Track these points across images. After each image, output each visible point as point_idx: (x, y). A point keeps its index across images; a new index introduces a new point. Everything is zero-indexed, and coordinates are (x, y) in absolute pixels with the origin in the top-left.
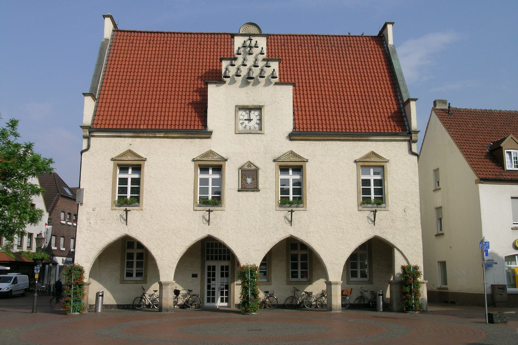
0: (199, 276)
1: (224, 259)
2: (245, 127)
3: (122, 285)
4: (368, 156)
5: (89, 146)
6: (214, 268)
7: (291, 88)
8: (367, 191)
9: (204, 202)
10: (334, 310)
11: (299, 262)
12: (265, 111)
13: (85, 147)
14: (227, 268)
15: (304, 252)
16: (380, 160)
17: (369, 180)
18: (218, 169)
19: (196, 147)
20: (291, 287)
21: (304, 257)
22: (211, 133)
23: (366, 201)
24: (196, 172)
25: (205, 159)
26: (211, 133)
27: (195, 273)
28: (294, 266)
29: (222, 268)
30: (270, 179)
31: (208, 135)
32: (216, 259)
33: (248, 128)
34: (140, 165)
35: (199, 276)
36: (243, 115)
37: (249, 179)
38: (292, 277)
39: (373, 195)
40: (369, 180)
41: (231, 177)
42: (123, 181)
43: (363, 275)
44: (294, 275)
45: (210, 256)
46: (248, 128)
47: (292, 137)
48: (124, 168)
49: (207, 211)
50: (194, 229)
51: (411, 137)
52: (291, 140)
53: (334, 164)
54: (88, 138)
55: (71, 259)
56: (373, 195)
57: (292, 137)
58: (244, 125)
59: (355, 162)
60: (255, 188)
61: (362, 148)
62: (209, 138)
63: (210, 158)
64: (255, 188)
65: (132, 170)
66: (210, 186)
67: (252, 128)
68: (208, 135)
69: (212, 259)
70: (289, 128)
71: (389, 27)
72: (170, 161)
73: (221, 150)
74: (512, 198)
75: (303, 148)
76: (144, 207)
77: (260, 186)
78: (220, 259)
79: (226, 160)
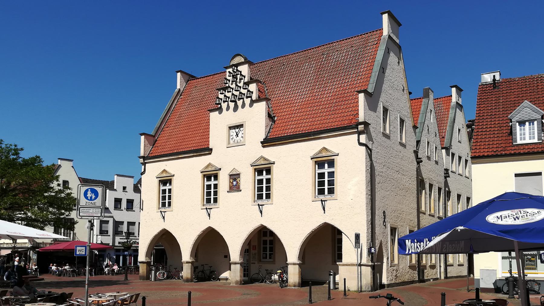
4: (320, 152)
5: (145, 169)
8: (321, 184)
13: (143, 171)
15: (272, 238)
16: (329, 154)
19: (200, 163)
22: (211, 149)
26: (211, 149)
28: (265, 249)
30: (248, 181)
31: (208, 151)
33: (236, 141)
36: (233, 132)
39: (325, 186)
41: (224, 182)
42: (321, 175)
46: (236, 141)
48: (209, 178)
52: (264, 147)
53: (294, 162)
54: (144, 164)
56: (325, 186)
57: (267, 142)
61: (312, 147)
62: (210, 154)
67: (239, 141)
68: (208, 151)
70: (262, 137)
72: (187, 172)
74: (517, 175)
75: (272, 153)
79: (220, 169)
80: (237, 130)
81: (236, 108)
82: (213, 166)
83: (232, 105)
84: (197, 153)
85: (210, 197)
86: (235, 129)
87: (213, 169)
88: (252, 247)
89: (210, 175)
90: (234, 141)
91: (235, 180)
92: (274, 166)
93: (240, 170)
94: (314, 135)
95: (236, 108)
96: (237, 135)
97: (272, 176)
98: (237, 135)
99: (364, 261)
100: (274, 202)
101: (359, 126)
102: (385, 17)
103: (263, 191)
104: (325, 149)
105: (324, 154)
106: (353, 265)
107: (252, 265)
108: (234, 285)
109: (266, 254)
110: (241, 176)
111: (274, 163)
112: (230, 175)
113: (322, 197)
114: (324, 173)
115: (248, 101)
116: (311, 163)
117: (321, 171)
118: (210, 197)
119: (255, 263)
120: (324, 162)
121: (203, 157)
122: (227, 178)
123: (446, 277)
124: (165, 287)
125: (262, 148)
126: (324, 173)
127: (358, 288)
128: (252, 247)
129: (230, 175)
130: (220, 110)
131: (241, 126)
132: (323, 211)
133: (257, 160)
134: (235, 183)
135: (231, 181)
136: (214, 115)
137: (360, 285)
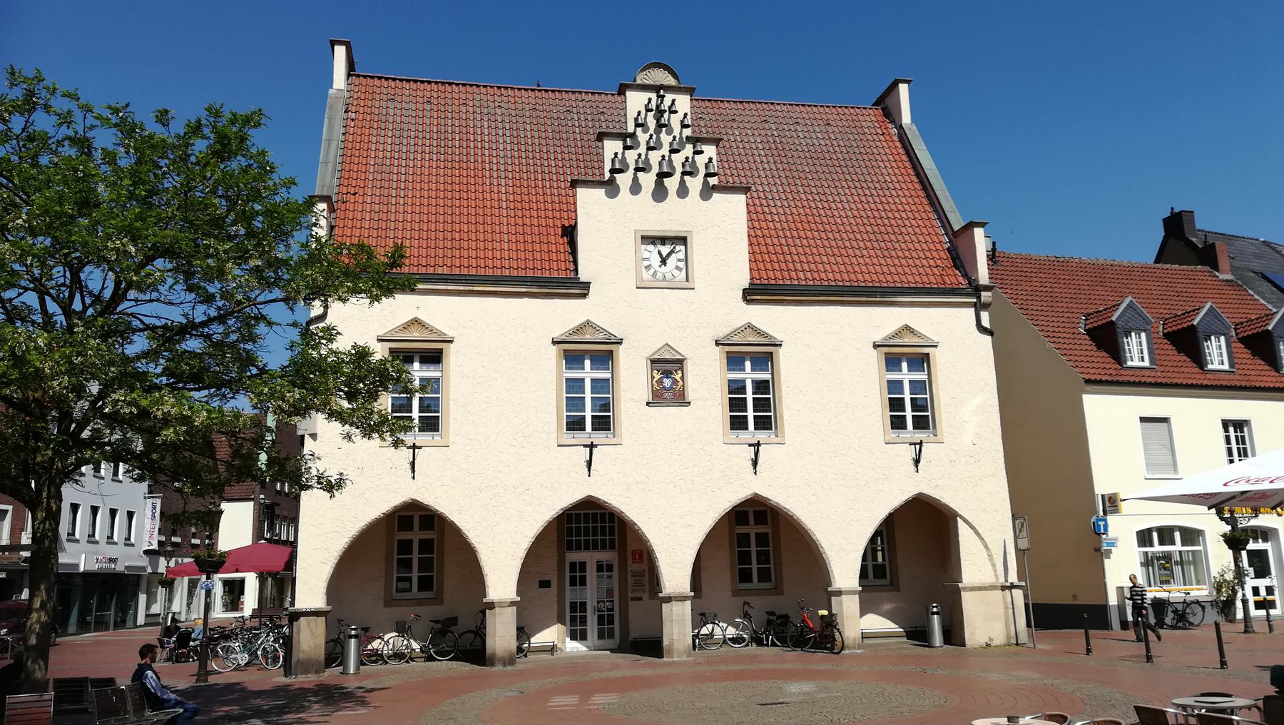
0: (554, 584)
1: (604, 548)
2: (655, 274)
3: (388, 610)
4: (897, 334)
6: (583, 566)
7: (740, 199)
8: (761, 405)
9: (575, 425)
10: (849, 648)
11: (415, 556)
12: (694, 242)
14: (610, 568)
16: (916, 341)
17: (901, 382)
18: (604, 358)
19: (561, 315)
20: (740, 600)
21: (426, 546)
22: (586, 285)
23: (575, 425)
24: (558, 365)
25: (897, 341)
26: (586, 285)
27: (547, 578)
28: (405, 565)
29: (600, 568)
30: (707, 380)
31: (581, 289)
32: (587, 548)
33: (659, 276)
34: (440, 351)
35: (554, 584)
36: (652, 253)
37: (668, 380)
38: (741, 581)
39: (911, 412)
40: (901, 382)
41: (632, 378)
42: (895, 386)
43: (764, 575)
44: (745, 576)
45: (590, 543)
46: (659, 276)
47: (752, 294)
49: (585, 446)
50: (560, 482)
51: (979, 297)
53: (827, 351)
55: (1155, 535)
56: (911, 412)
57: (752, 294)
58: (652, 271)
59: (876, 346)
60: (680, 399)
61: (884, 320)
62: (584, 296)
63: (588, 337)
64: (680, 399)
65: (752, 365)
66: (588, 395)
67: (668, 276)
68: (581, 289)
69: (578, 548)
71: (903, 89)
73: (610, 323)
74: (1143, 420)
75: (774, 319)
76: (452, 439)
77: (690, 395)
78: (595, 548)
79: (620, 342)
80: (665, 250)
81: (660, 193)
82: (597, 329)
83: (648, 180)
84: (867, 296)
85: (591, 417)
86: (653, 243)
87: (599, 337)
88: (629, 556)
89: (588, 352)
90: (655, 274)
91: (667, 374)
92: (621, 348)
93: (683, 350)
94: (883, 294)
95: (660, 193)
96: (664, 262)
97: (559, 374)
98: (664, 262)
99: (1013, 578)
100: (786, 440)
101: (983, 294)
102: (340, 51)
103: (753, 409)
104: (907, 328)
105: (908, 340)
106: (992, 588)
107: (630, 603)
108: (684, 658)
109: (410, 580)
110: (689, 367)
111: (451, 342)
112: (653, 361)
113: (744, 436)
114: (582, 380)
115: (695, 184)
116: (552, 355)
117: (894, 376)
118: (591, 417)
119: (641, 599)
120: (905, 355)
121: (526, 300)
122: (644, 367)
123: (1065, 612)
124: (723, 668)
125: (743, 304)
126: (582, 380)
127: (1008, 637)
128: (629, 556)
129: (653, 361)
130: (611, 187)
131: (683, 240)
132: (410, 475)
133: (737, 332)
134: (667, 382)
135: (657, 377)
136: (589, 200)
137: (1013, 632)
